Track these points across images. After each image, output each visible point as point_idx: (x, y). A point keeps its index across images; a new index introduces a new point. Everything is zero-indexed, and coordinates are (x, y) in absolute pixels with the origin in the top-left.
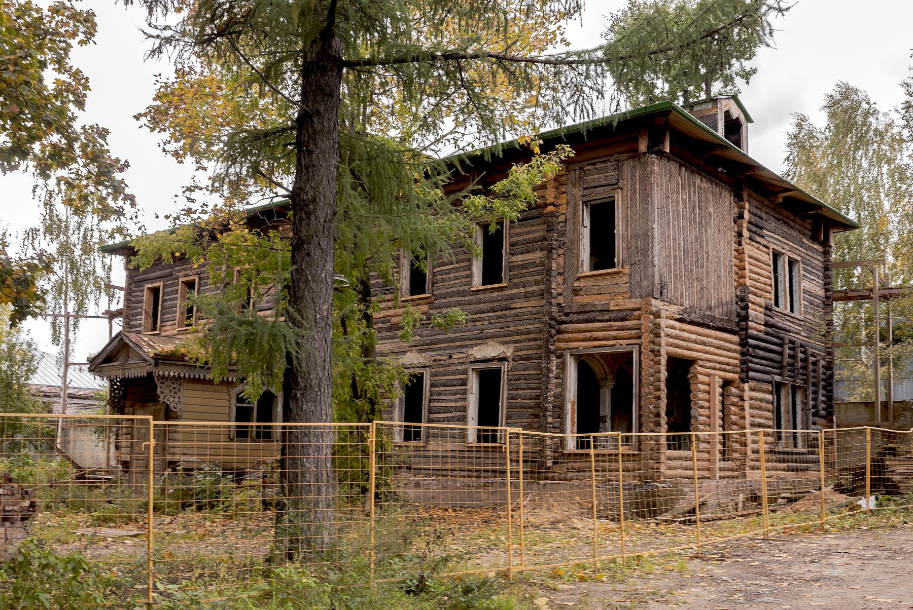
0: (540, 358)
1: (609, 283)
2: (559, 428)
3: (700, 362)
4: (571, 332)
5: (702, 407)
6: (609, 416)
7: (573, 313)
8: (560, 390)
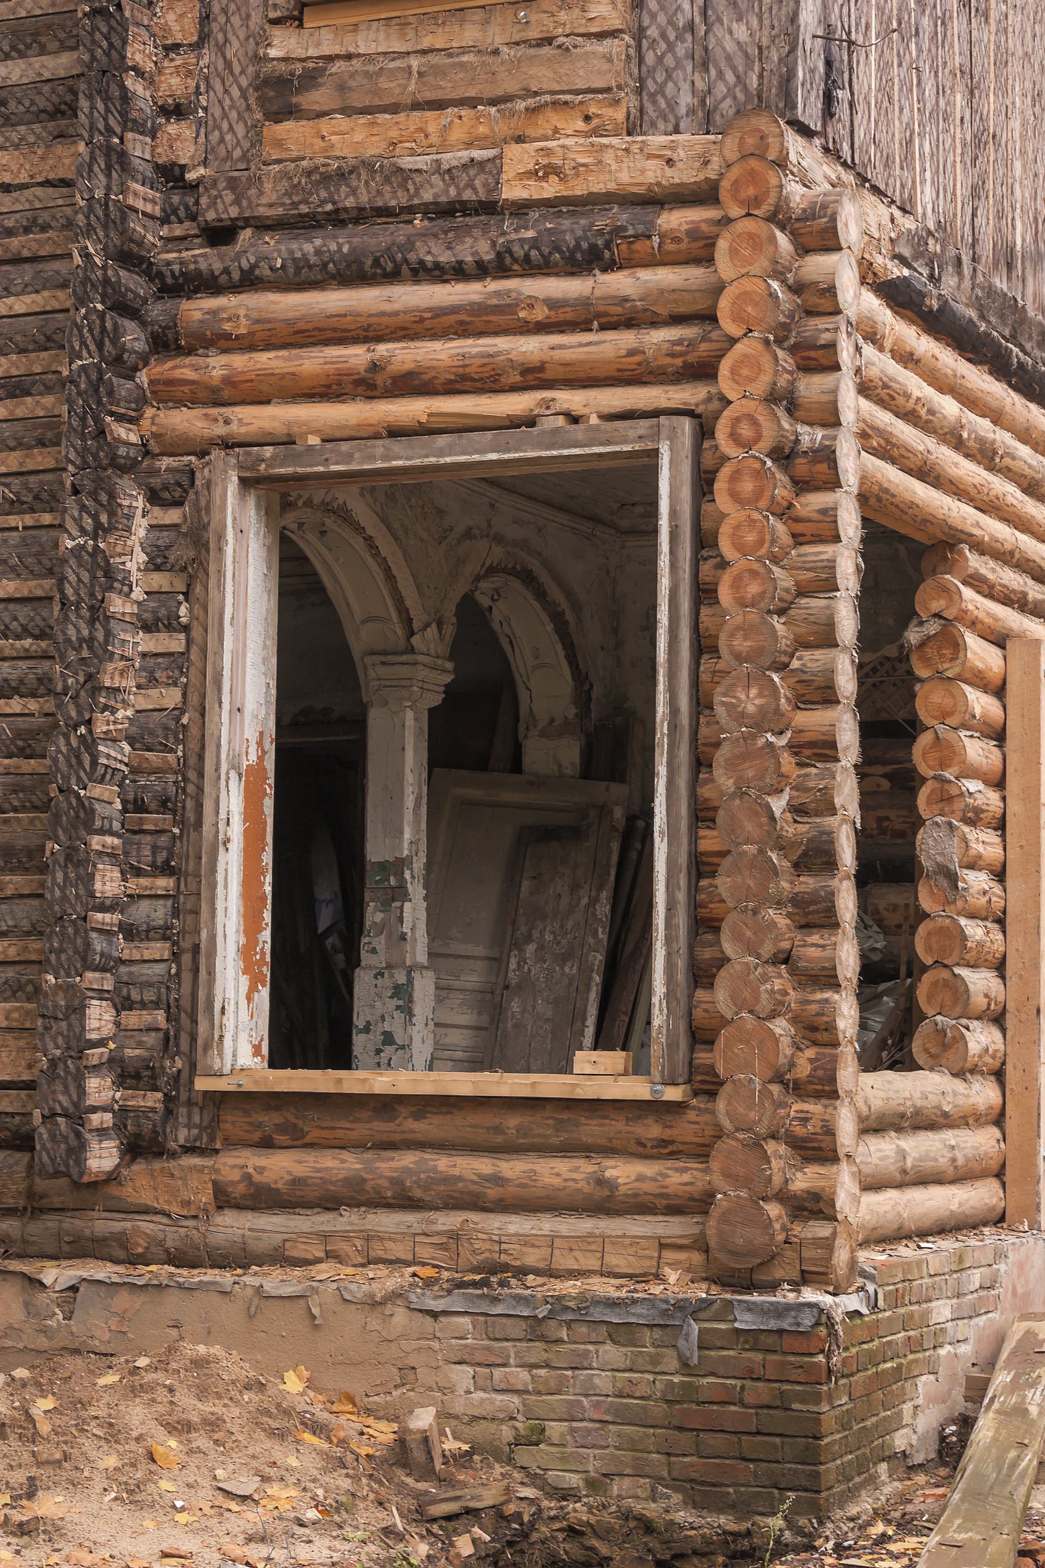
0: (48, 500)
1: (497, 35)
2: (164, 933)
3: (975, 562)
4: (248, 344)
5: (974, 818)
6: (419, 863)
7: (263, 226)
8: (172, 697)
